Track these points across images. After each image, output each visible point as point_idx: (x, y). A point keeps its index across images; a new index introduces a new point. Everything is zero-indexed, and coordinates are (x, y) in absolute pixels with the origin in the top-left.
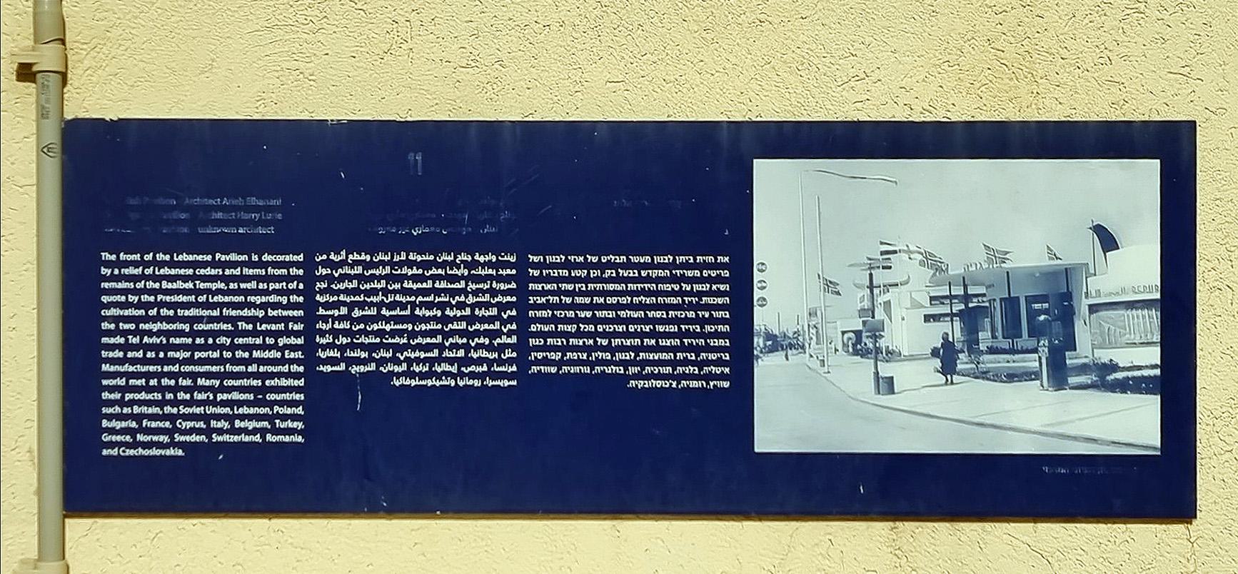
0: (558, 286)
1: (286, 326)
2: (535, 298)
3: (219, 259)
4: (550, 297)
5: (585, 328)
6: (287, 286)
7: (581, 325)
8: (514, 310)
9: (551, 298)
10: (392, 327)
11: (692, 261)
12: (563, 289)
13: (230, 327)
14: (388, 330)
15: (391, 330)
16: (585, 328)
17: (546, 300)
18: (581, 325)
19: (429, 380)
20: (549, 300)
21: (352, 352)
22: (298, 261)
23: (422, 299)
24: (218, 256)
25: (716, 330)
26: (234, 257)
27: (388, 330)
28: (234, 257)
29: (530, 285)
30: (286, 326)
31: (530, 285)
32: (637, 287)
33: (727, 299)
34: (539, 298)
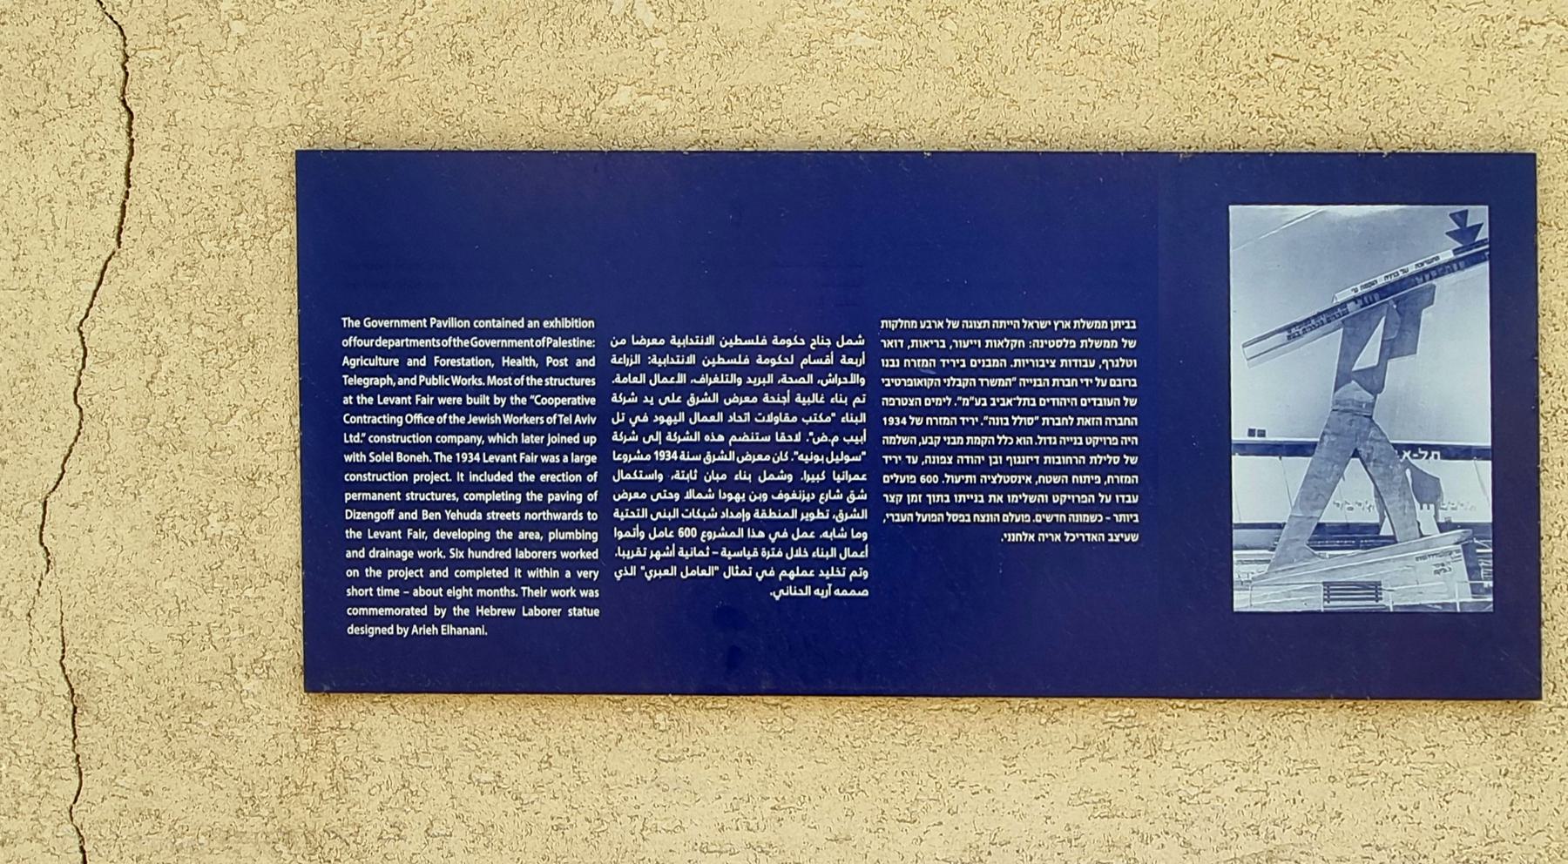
0: (942, 382)
1: (431, 611)
2: (998, 400)
3: (435, 325)
4: (1018, 398)
5: (1071, 537)
6: (512, 382)
7: (1066, 534)
8: (548, 363)
9: (1020, 400)
10: (798, 574)
11: (964, 366)
12: (949, 385)
13: (538, 536)
14: (792, 579)
15: (796, 578)
16: (1071, 537)
17: (1013, 402)
18: (1066, 534)
19: (789, 340)
20: (1018, 401)
21: (838, 571)
22: (518, 328)
23: (736, 440)
24: (433, 321)
25: (962, 481)
26: (452, 323)
27: (792, 579)
28: (452, 323)
29: (883, 322)
30: (431, 611)
31: (883, 322)
32: (1073, 363)
33: (1136, 439)
34: (1003, 399)
